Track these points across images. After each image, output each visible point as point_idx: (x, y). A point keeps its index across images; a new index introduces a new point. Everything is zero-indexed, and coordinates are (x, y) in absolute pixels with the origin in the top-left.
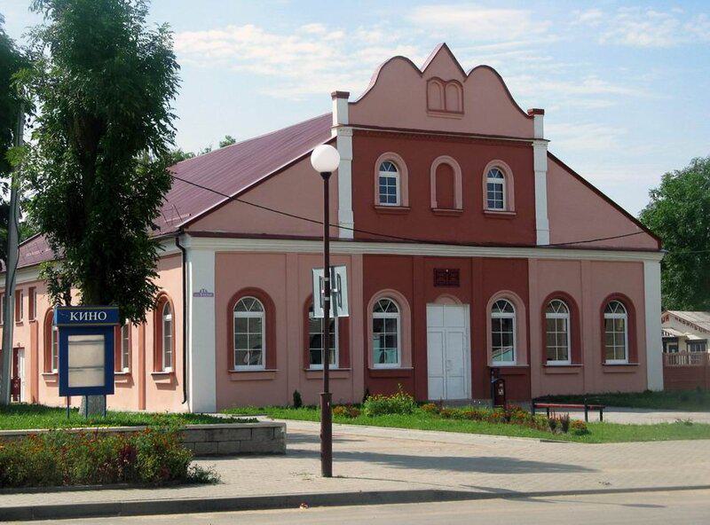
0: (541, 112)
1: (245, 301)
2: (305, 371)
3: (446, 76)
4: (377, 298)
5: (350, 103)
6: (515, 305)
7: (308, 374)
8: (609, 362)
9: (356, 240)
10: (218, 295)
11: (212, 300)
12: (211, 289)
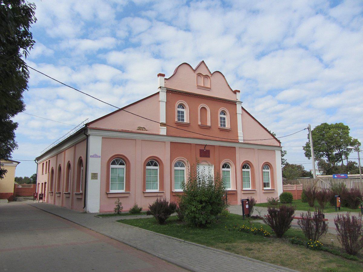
0: (239, 91)
1: (116, 160)
2: (144, 193)
3: (201, 71)
4: (175, 161)
5: (165, 79)
6: (158, 162)
7: (109, 195)
8: (147, 191)
9: (167, 135)
10: (102, 157)
11: (100, 159)
12: (99, 154)
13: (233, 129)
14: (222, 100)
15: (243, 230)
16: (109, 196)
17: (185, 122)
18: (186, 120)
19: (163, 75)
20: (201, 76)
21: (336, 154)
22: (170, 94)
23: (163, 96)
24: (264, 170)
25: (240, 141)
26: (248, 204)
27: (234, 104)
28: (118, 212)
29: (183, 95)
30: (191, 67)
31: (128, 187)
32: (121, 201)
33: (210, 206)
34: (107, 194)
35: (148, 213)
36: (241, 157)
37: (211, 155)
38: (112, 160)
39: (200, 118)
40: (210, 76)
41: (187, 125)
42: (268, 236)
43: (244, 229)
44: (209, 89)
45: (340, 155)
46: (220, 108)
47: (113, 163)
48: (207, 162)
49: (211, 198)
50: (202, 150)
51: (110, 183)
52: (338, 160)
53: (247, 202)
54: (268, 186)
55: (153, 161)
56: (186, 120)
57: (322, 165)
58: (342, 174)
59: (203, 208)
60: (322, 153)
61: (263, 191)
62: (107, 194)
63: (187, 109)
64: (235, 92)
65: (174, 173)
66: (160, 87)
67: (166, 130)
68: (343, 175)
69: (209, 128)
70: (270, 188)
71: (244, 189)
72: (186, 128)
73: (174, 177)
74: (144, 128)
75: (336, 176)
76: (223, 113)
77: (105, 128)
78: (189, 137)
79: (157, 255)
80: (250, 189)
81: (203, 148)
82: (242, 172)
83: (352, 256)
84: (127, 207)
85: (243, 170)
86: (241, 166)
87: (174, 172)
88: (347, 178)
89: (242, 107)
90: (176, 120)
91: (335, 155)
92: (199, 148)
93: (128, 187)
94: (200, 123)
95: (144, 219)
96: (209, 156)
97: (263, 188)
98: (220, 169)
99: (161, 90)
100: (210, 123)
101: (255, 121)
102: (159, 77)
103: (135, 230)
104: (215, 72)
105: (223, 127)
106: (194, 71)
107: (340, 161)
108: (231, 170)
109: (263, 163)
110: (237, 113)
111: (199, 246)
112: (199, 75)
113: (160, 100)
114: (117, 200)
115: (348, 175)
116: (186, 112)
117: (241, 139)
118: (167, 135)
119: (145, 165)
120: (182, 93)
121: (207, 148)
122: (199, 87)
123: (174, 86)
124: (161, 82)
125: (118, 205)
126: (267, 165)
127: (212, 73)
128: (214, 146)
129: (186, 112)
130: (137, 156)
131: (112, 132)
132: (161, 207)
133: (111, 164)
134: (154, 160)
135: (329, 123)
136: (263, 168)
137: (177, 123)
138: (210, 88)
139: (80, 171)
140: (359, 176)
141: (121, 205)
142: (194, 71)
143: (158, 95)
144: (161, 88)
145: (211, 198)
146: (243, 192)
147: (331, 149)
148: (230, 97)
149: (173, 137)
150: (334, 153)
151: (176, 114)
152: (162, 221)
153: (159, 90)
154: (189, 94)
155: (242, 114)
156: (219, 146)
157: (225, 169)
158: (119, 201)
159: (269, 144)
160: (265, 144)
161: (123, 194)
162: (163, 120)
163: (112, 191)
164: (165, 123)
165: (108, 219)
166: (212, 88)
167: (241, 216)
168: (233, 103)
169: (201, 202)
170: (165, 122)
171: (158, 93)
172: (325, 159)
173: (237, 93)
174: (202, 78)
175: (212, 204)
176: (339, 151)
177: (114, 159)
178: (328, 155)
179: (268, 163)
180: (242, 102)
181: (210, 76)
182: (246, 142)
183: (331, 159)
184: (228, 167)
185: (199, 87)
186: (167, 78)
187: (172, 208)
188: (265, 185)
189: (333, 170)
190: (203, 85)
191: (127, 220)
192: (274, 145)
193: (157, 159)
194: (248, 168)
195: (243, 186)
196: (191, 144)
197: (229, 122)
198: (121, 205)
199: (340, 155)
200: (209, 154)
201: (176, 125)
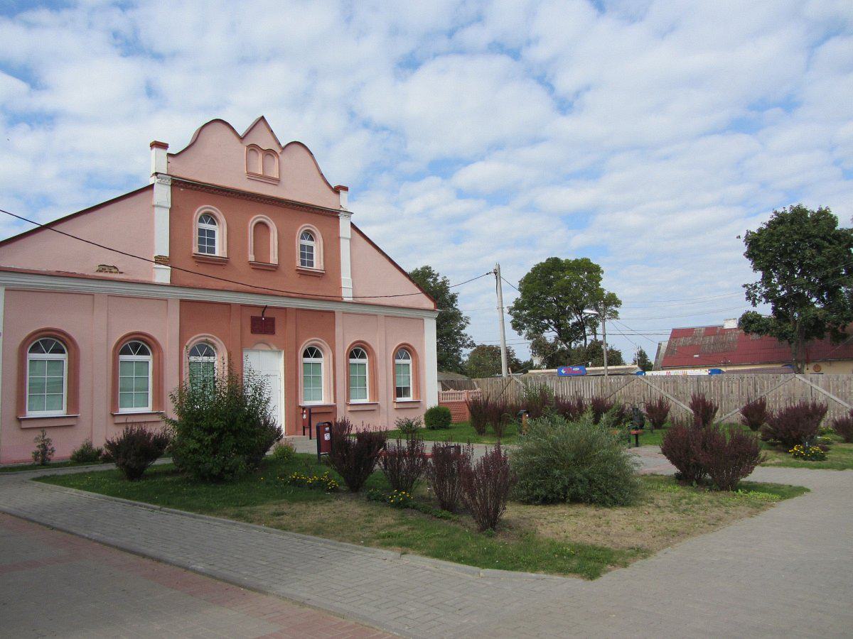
0: (346, 189)
2: (114, 416)
4: (192, 342)
5: (169, 155)
6: (148, 345)
13: (330, 275)
14: (307, 207)
15: (294, 482)
16: (25, 425)
17: (217, 254)
18: (220, 250)
19: (164, 146)
20: (257, 152)
21: (574, 324)
22: (182, 190)
23: (163, 194)
24: (398, 361)
25: (345, 299)
26: (330, 431)
27: (333, 216)
28: (43, 460)
29: (212, 193)
30: (232, 128)
31: (73, 403)
32: (49, 435)
33: (232, 437)
34: (20, 420)
35: (107, 459)
36: (346, 336)
37: (278, 330)
38: (32, 342)
39: (252, 246)
40: (278, 151)
41: (222, 262)
42: (335, 490)
43: (295, 479)
44: (276, 181)
45: (580, 326)
46: (299, 225)
47: (36, 349)
48: (267, 344)
49: (233, 422)
50: (256, 317)
51: (28, 394)
52: (578, 338)
53: (327, 429)
54: (408, 396)
55: (138, 344)
56: (220, 250)
57: (539, 347)
58: (577, 366)
59: (216, 442)
60: (546, 321)
61: (395, 406)
62: (20, 420)
63: (221, 225)
64: (337, 190)
65: (302, 369)
66: (156, 174)
67: (169, 273)
68: (576, 369)
69: (274, 269)
70: (410, 399)
71: (353, 401)
72: (217, 272)
73: (302, 377)
74: (115, 268)
75: (563, 371)
76: (309, 235)
77: (13, 267)
78: (226, 289)
79: (87, 535)
80: (367, 401)
81: (258, 314)
82: (349, 365)
83: (445, 513)
84: (64, 447)
85: (352, 361)
86: (347, 354)
87: (302, 366)
88: (584, 374)
89: (352, 223)
90: (195, 250)
91: (572, 326)
92: (249, 313)
93: (73, 403)
94: (251, 258)
95: (97, 472)
96: (273, 332)
97: (394, 399)
98: (297, 359)
99: (157, 180)
100: (276, 257)
101: (380, 255)
102: (154, 149)
103: (71, 494)
104: (288, 144)
105: (306, 268)
106: (242, 139)
107: (581, 339)
108: (324, 361)
109: (396, 346)
110: (339, 238)
111: (186, 515)
112: (253, 148)
113: (155, 203)
114: (38, 433)
115: (587, 369)
116: (220, 233)
117: (347, 294)
118: (173, 285)
119: (117, 354)
120: (210, 188)
121: (268, 314)
122: (252, 176)
123: (189, 171)
124: (157, 161)
125: (44, 445)
126: (405, 350)
127: (283, 145)
128: (285, 309)
129: (220, 233)
130: (95, 331)
131: (30, 277)
132: (132, 444)
133: (30, 352)
134: (140, 340)
135: (563, 258)
136: (396, 356)
137: (200, 260)
138: (278, 180)
139: (26, 363)
140: (603, 370)
141: (50, 444)
142: (242, 139)
143: (148, 193)
144: (159, 175)
145: (233, 422)
146: (349, 408)
147: (566, 315)
148: (324, 200)
149: (185, 289)
150: (571, 322)
151: (196, 237)
152: (134, 473)
153: (152, 180)
154: (228, 192)
155: (351, 240)
156: (297, 309)
157: (311, 360)
158: (43, 436)
159: (411, 306)
160: (403, 305)
161: (61, 420)
162: (163, 249)
163: (31, 414)
164: (168, 255)
165: (15, 476)
166: (283, 180)
167: (312, 455)
168: (333, 215)
169: (210, 430)
170: (166, 254)
171: (151, 187)
172: (550, 335)
173: (342, 192)
174: (260, 155)
175: (235, 433)
176: (579, 318)
177: (36, 339)
178: (558, 326)
179: (403, 346)
180: (352, 213)
181: (278, 151)
182: (360, 300)
183: (566, 334)
184: (318, 355)
185: (252, 176)
186: (174, 152)
187: (157, 446)
188: (400, 392)
189: (561, 358)
190: (260, 172)
191: (58, 476)
192: (421, 307)
193: (146, 338)
194: (363, 356)
195: (351, 397)
196: (229, 304)
197: (322, 257)
198: (50, 444)
199: (580, 326)
200: (273, 325)
201: (193, 262)
